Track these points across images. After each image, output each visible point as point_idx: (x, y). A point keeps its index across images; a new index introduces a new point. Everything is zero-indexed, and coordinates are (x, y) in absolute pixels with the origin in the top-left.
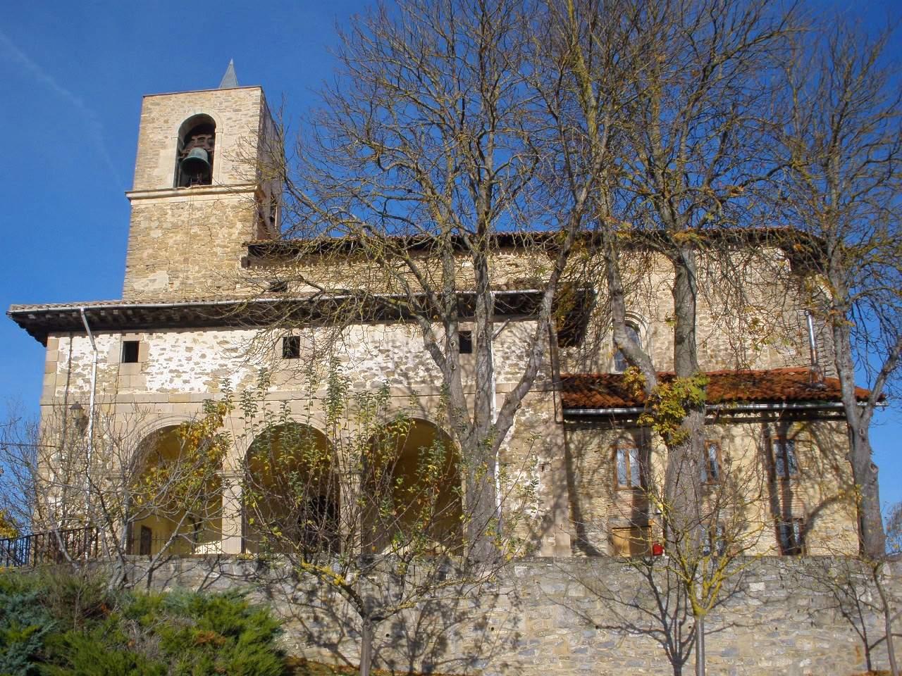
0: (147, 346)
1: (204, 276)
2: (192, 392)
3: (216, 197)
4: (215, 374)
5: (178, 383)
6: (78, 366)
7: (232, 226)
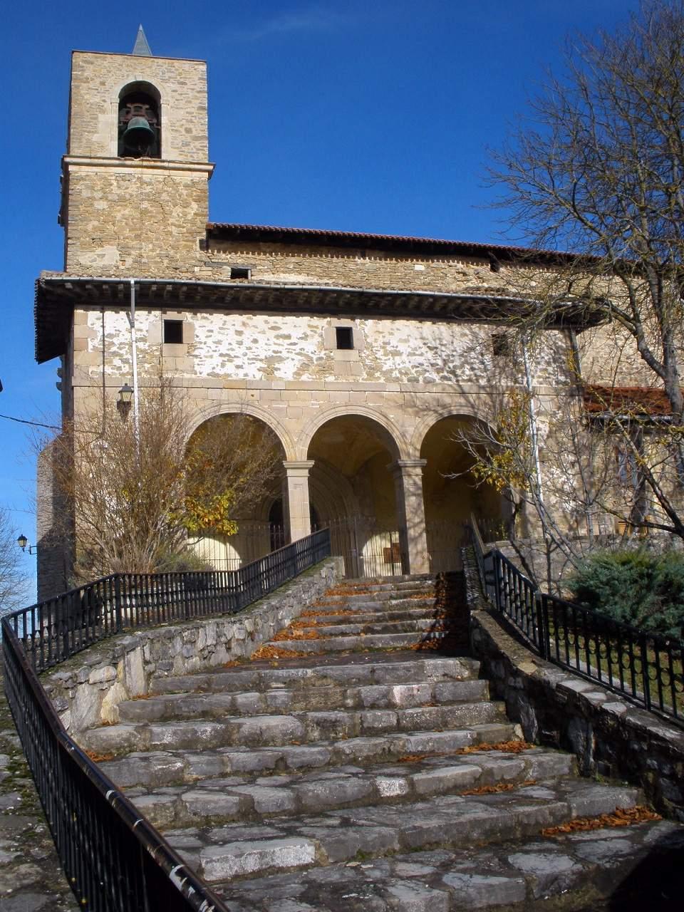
0: (191, 326)
1: (159, 256)
2: (248, 378)
3: (166, 172)
4: (269, 360)
5: (230, 368)
6: (113, 344)
7: (186, 205)
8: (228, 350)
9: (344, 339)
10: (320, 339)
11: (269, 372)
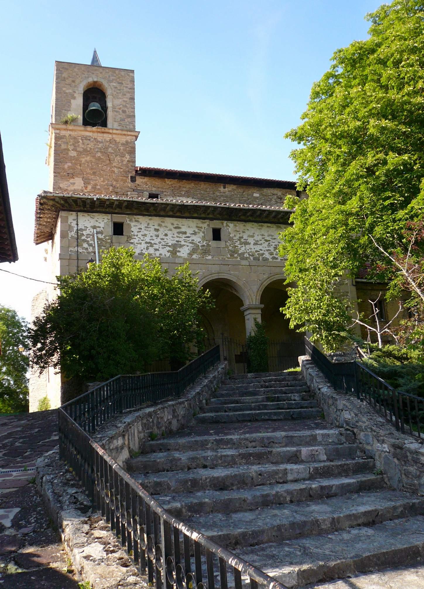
0: (129, 226)
1: (107, 185)
6: (83, 235)
9: (217, 235)
10: (203, 235)
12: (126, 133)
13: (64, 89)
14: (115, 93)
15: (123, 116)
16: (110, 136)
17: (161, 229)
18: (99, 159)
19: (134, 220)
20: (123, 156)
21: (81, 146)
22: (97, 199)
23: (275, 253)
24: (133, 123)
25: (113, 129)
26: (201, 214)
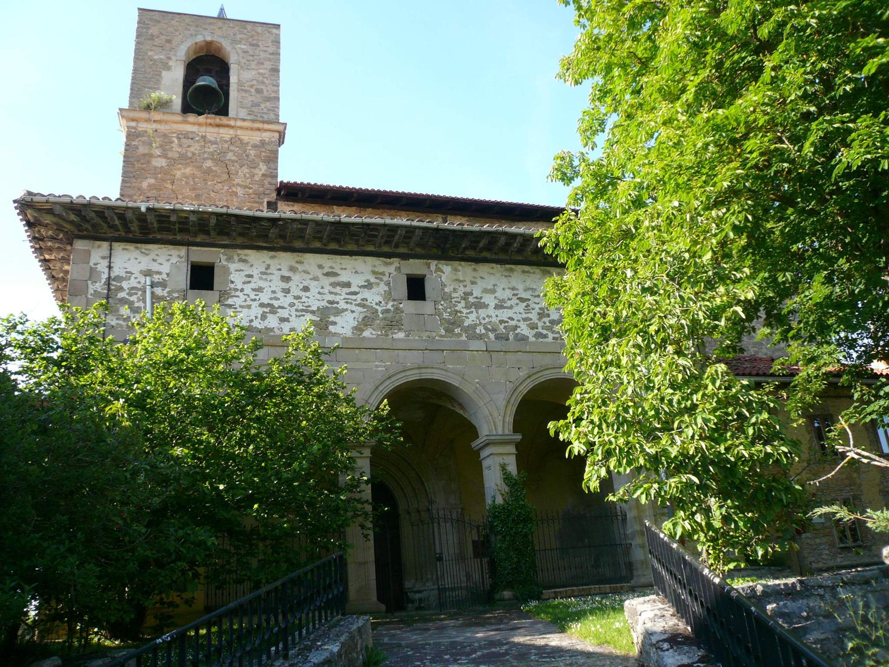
0: (227, 271)
5: (272, 322)
6: (121, 289)
8: (271, 299)
9: (416, 289)
10: (386, 288)
11: (323, 325)
12: (260, 126)
13: (150, 53)
14: (245, 61)
15: (257, 98)
16: (231, 132)
17: (296, 278)
18: (209, 171)
19: (236, 258)
20: (253, 166)
21: (176, 149)
22: (148, 209)
23: (540, 324)
24: (275, 110)
25: (236, 119)
26: (380, 246)
